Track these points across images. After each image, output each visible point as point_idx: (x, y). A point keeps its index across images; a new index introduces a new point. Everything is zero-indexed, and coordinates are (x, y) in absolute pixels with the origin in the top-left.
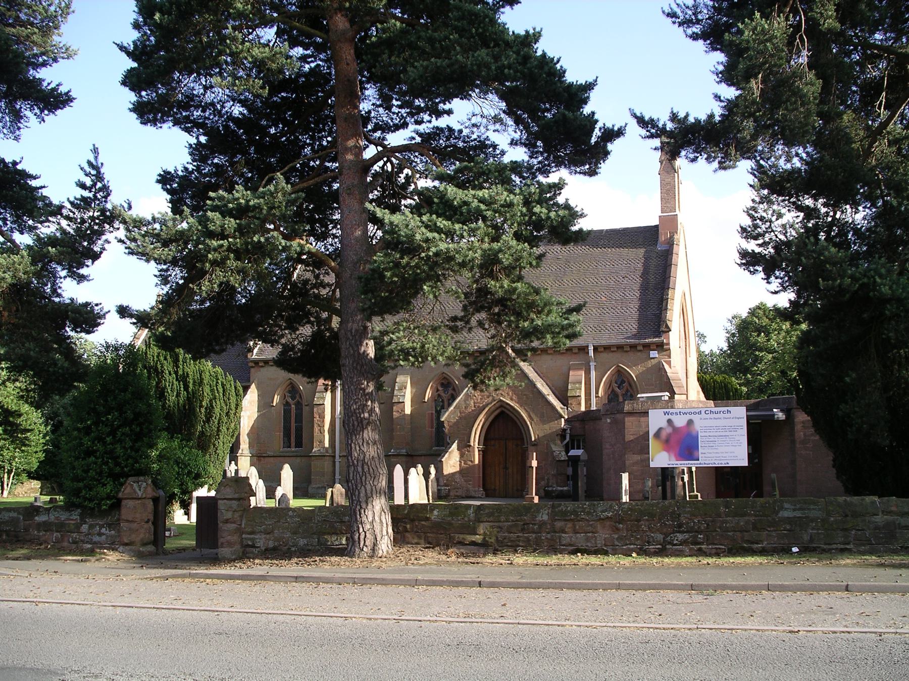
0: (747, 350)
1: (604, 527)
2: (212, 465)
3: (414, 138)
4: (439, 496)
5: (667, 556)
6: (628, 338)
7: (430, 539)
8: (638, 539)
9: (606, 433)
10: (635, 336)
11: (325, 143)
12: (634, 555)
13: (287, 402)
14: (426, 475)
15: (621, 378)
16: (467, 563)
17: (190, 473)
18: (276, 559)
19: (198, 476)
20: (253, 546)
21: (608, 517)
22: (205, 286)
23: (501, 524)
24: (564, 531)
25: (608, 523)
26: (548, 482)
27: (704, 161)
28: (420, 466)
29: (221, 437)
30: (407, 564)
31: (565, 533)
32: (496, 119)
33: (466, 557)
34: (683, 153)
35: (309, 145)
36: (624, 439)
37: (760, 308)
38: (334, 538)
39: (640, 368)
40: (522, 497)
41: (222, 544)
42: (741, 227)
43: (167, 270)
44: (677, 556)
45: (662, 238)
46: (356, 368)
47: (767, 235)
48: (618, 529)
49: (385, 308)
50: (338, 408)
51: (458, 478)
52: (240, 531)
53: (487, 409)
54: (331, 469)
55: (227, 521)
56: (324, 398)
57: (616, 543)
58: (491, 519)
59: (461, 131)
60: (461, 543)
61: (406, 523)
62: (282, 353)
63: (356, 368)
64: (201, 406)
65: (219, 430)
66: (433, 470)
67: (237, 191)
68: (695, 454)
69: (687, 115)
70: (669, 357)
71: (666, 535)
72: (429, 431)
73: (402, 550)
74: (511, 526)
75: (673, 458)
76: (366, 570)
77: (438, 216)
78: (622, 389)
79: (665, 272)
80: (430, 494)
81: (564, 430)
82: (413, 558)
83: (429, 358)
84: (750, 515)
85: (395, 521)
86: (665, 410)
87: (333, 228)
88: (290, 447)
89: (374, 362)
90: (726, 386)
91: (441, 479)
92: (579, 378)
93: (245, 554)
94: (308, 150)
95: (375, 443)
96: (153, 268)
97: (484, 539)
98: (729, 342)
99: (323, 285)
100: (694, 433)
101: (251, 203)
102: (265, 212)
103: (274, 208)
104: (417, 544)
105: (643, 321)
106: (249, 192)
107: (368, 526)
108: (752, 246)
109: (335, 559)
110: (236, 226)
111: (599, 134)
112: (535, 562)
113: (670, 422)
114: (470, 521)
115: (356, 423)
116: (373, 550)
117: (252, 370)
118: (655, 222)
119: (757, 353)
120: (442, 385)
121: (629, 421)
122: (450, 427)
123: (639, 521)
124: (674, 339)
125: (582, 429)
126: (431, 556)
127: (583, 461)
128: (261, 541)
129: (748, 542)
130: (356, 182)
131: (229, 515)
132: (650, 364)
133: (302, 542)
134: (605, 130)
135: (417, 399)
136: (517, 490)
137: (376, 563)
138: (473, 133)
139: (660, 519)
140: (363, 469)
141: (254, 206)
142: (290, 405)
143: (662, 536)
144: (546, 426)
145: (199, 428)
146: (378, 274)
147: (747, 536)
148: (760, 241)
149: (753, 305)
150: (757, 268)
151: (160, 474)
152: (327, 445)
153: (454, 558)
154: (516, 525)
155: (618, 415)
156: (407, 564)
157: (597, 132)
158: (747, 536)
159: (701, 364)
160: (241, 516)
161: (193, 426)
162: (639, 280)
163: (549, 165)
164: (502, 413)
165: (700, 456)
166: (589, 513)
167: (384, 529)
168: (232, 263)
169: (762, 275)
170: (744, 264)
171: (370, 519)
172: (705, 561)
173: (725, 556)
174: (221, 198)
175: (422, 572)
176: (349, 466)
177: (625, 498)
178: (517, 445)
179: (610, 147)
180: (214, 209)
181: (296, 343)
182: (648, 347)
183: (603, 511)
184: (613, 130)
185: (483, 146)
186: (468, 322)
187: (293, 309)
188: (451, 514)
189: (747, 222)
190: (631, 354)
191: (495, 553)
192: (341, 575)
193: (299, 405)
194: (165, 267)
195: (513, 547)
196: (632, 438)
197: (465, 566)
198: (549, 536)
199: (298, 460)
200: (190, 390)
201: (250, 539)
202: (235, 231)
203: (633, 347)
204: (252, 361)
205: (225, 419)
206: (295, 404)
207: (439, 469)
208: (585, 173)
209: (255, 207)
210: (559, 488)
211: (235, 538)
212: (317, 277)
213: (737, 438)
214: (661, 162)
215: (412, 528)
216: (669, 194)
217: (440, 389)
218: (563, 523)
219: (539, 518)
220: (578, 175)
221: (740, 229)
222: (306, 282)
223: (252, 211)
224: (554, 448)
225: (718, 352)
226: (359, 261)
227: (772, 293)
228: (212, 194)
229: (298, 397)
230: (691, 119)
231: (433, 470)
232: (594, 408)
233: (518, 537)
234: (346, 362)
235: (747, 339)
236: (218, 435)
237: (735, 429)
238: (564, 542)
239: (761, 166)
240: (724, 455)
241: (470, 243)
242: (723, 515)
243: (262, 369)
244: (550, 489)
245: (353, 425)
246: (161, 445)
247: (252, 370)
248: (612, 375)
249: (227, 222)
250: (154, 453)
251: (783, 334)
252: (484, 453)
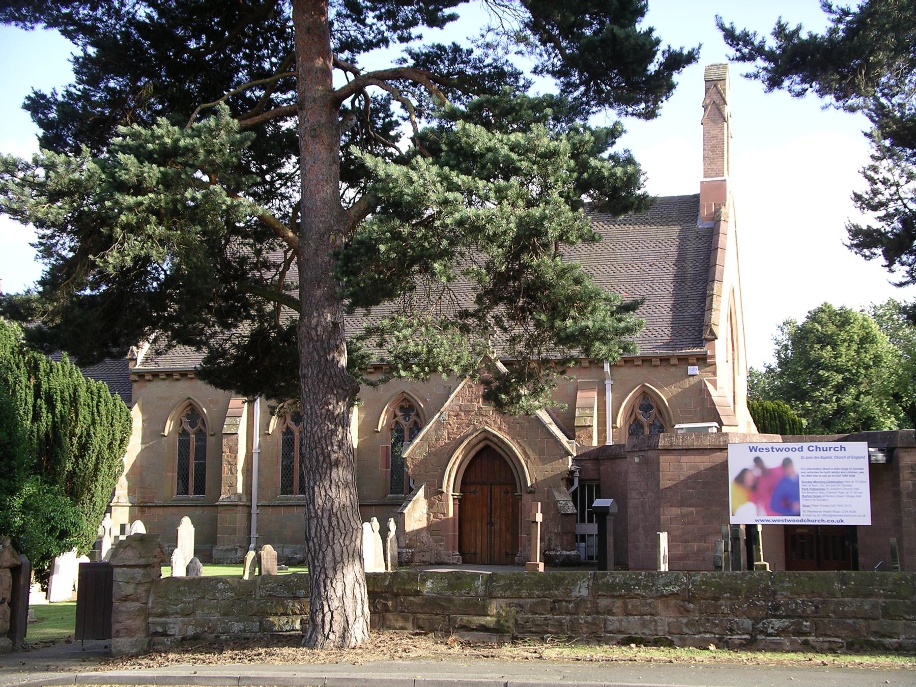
0: (806, 368)
1: (667, 607)
2: (84, 518)
3: (405, 61)
4: (400, 562)
5: (760, 651)
6: (658, 348)
7: (421, 622)
8: (717, 625)
9: (633, 478)
10: (667, 345)
11: (267, 66)
12: (712, 647)
13: (184, 430)
14: (384, 532)
15: (647, 403)
16: (477, 656)
17: (53, 529)
18: (201, 653)
19: (64, 534)
20: (165, 634)
21: (673, 594)
22: (113, 257)
23: (522, 601)
24: (610, 612)
25: (673, 602)
26: (549, 544)
27: (815, 95)
28: (375, 519)
29: (100, 478)
30: (392, 657)
31: (613, 614)
32: (520, 39)
33: (475, 647)
34: (786, 83)
35: (244, 67)
36: (658, 485)
37: (823, 311)
38: (284, 619)
39: (674, 389)
40: (522, 564)
41: (118, 631)
42: (855, 194)
43: (52, 237)
44: (774, 650)
45: (704, 212)
46: (322, 381)
47: (891, 204)
48: (687, 611)
49: (366, 298)
50: (257, 440)
51: (425, 536)
52: (145, 613)
53: (466, 442)
54: (245, 524)
55: (126, 599)
56: (237, 425)
57: (685, 630)
58: (508, 593)
59: (470, 52)
60: (466, 628)
61: (386, 599)
62: (207, 360)
63: (322, 381)
64: (73, 434)
65: (97, 469)
66: (392, 526)
67: (159, 126)
68: (795, 506)
69: (799, 28)
70: (715, 374)
71: (756, 621)
72: (383, 471)
73: (382, 638)
74: (535, 604)
75: (763, 511)
76: (336, 667)
77: (452, 168)
78: (649, 419)
79: (708, 258)
80: (389, 559)
81: (572, 473)
82: (400, 649)
83: (440, 368)
84: (878, 595)
85: (373, 595)
87: (282, 185)
88: (291, 492)
89: (346, 372)
90: (780, 416)
91: (401, 539)
92: (589, 401)
93: (153, 645)
94: (242, 75)
95: (346, 485)
96: (31, 233)
97: (498, 622)
98: (779, 357)
99: (266, 265)
100: (792, 477)
101: (182, 143)
102: (202, 157)
103: (213, 152)
104: (403, 628)
105: (677, 325)
106: (176, 128)
107: (335, 604)
108: (869, 220)
109: (287, 651)
110: (159, 175)
111: (662, 60)
112: (573, 656)
113: (758, 461)
114: (477, 596)
115: (321, 458)
116: (343, 637)
117: (135, 385)
118: (696, 190)
119: (821, 372)
120: (402, 408)
121: (665, 461)
122: (415, 466)
123: (716, 599)
124: (720, 350)
125: (595, 474)
126: (425, 646)
127: (613, 515)
128: (177, 627)
129: (876, 633)
130: (323, 120)
131: (129, 589)
132: (688, 383)
133: (237, 627)
134: (670, 54)
135: (368, 428)
136: (507, 554)
137: (348, 657)
138: (487, 56)
139: (747, 598)
140: (330, 522)
141: (186, 147)
142: (188, 435)
143: (751, 622)
144: (548, 467)
145: (69, 466)
146: (368, 247)
147: (874, 625)
148: (882, 213)
149: (814, 306)
150: (874, 250)
151: (23, 532)
152: (240, 490)
153: (457, 648)
154: (543, 603)
155: (650, 453)
156: (392, 657)
157: (659, 58)
158: (874, 625)
159: (752, 387)
160: (148, 591)
161: (59, 462)
162: (672, 270)
163: (588, 103)
164: (487, 447)
165: (802, 509)
166: (645, 587)
167: (359, 607)
168: (154, 229)
169: (882, 260)
170: (856, 246)
171: (339, 593)
172: (819, 659)
173: (845, 654)
174: (135, 136)
175: (419, 670)
176: (309, 519)
177: (664, 567)
178: (506, 493)
179: (676, 77)
180: (125, 149)
181: (227, 346)
182: (684, 360)
183: (666, 585)
184: (681, 54)
185: (500, 74)
186: (482, 319)
187: (226, 298)
188: (451, 586)
189: (864, 187)
190: (662, 370)
191: (514, 641)
192: (304, 675)
193: (201, 435)
194: (49, 232)
195: (540, 634)
196: (669, 484)
197: (474, 661)
198: (589, 619)
199: (199, 511)
200: (57, 411)
201: (160, 624)
202: (158, 183)
203: (665, 360)
204: (134, 373)
205: (106, 454)
206: (196, 434)
207: (400, 524)
208: (639, 115)
209: (187, 149)
210: (565, 553)
211: (138, 623)
212: (258, 253)
213: (855, 485)
214: (705, 107)
215: (395, 607)
216: (715, 151)
217: (399, 414)
218: (609, 600)
219: (575, 593)
220: (629, 117)
221: (853, 196)
222: (243, 260)
223: (182, 155)
224: (558, 497)
225: (763, 370)
226: (328, 230)
227: (896, 285)
228: (122, 129)
229: (199, 425)
230: (804, 35)
231: (392, 526)
232: (609, 442)
233: (546, 619)
234: (308, 371)
235: (805, 353)
236: (96, 476)
237: (852, 472)
238: (611, 628)
239: (882, 106)
240: (837, 509)
241: (490, 207)
242: (839, 595)
243: (149, 385)
244: (552, 553)
245: (317, 461)
246: (28, 489)
247: (135, 385)
248: (635, 398)
249: (146, 169)
250: (18, 502)
251: (855, 347)
252: (461, 503)
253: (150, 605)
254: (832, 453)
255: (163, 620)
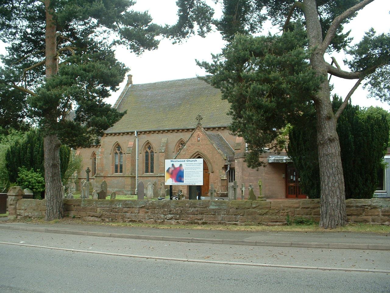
55: (11, 205)
68: (182, 179)
86: (171, 160)
100: (182, 170)
113: (173, 165)
131: (12, 203)
253: (17, 207)
254: (193, 162)
255: (20, 211)
